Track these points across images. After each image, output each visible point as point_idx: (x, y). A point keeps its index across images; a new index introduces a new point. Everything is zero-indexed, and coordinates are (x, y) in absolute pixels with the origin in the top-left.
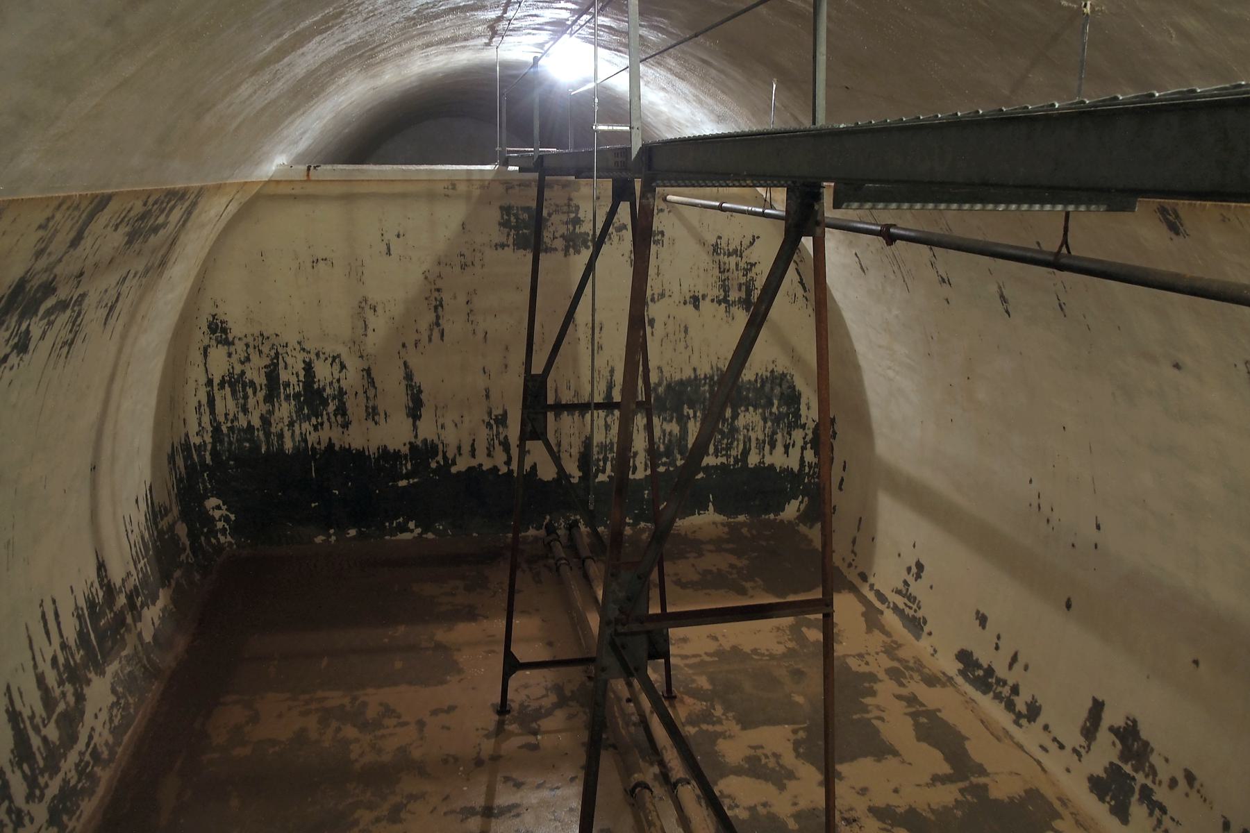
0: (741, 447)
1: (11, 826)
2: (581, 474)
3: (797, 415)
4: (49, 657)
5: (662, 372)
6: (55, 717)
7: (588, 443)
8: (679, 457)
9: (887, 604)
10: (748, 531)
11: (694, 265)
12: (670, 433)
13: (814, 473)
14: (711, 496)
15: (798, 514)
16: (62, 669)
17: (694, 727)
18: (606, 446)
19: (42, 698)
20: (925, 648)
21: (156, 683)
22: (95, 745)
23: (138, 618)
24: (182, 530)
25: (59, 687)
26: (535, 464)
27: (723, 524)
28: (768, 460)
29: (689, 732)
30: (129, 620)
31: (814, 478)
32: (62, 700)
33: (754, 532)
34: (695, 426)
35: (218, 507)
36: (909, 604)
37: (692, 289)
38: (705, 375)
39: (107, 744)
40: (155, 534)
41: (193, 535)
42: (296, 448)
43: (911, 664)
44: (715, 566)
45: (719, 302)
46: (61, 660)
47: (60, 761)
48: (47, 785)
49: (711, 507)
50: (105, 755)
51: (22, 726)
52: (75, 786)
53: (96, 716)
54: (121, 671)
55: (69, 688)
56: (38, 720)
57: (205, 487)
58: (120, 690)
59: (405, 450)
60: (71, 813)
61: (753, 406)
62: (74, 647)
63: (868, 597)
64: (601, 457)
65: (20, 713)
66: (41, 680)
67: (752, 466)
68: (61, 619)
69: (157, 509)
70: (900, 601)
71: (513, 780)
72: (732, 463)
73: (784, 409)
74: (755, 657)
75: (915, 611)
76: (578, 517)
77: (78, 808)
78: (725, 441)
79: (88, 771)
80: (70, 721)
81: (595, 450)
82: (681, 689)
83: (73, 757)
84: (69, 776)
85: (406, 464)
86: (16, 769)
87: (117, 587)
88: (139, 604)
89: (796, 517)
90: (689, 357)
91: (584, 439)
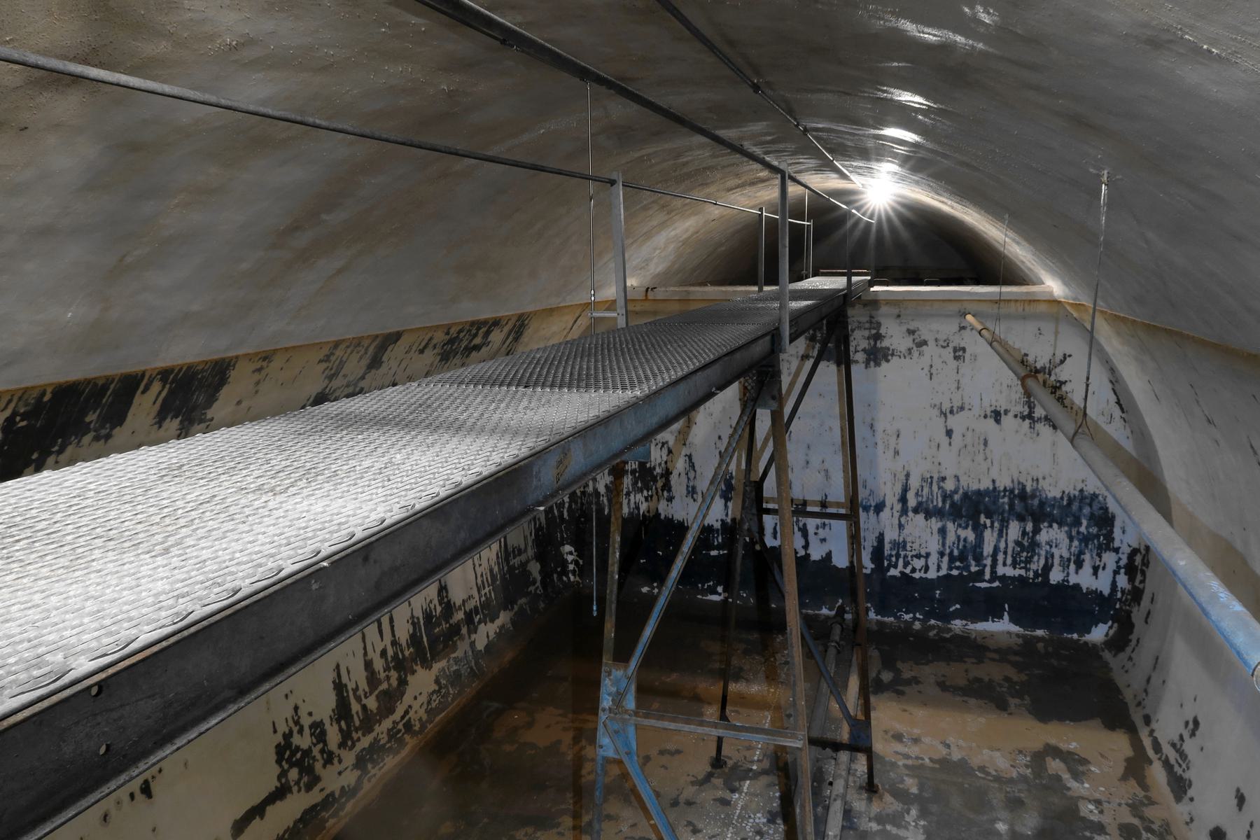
0: (1042, 562)
1: (321, 762)
2: (873, 566)
3: (1110, 537)
4: (378, 651)
5: (958, 481)
6: (376, 692)
7: (881, 538)
8: (973, 563)
9: (1160, 755)
10: (1044, 647)
11: (997, 381)
12: (965, 540)
13: (1126, 600)
14: (1006, 606)
15: (1106, 638)
16: (390, 659)
17: (879, 824)
18: (899, 544)
19: (367, 678)
20: (1182, 814)
21: (477, 682)
22: (410, 718)
23: (473, 629)
24: (535, 568)
25: (385, 672)
26: (830, 552)
27: (1018, 635)
28: (1073, 579)
29: (871, 827)
30: (464, 630)
31: (1125, 605)
32: (386, 682)
33: (1050, 649)
34: (992, 536)
35: (571, 553)
36: (1180, 761)
37: (994, 403)
38: (1005, 488)
39: (420, 720)
40: (506, 569)
41: (546, 574)
42: (631, 514)
43: (1155, 827)
44: (988, 675)
45: (1023, 418)
46: (390, 652)
47: (375, 725)
48: (359, 739)
49: (1006, 616)
50: (417, 728)
51: (345, 694)
52: (385, 744)
53: (415, 698)
54: (448, 668)
55: (394, 674)
56: (360, 692)
57: (562, 536)
58: (443, 682)
59: (717, 525)
60: (375, 763)
61: (1057, 523)
62: (404, 644)
63: (1144, 743)
64: (894, 553)
65: (346, 686)
66: (368, 665)
67: (1055, 583)
68: (395, 624)
69: (510, 549)
70: (1172, 755)
71: (694, 826)
72: (1031, 576)
73: (1094, 530)
74: (979, 775)
75: (1184, 771)
76: (869, 605)
77: (382, 761)
78: (1025, 554)
79: (398, 736)
80: (389, 699)
81: (887, 546)
82: (887, 787)
83: (387, 723)
84: (381, 736)
85: (717, 538)
86: (334, 724)
87: (457, 605)
88: (476, 620)
89: (1103, 641)
90: (989, 469)
91: (877, 535)
